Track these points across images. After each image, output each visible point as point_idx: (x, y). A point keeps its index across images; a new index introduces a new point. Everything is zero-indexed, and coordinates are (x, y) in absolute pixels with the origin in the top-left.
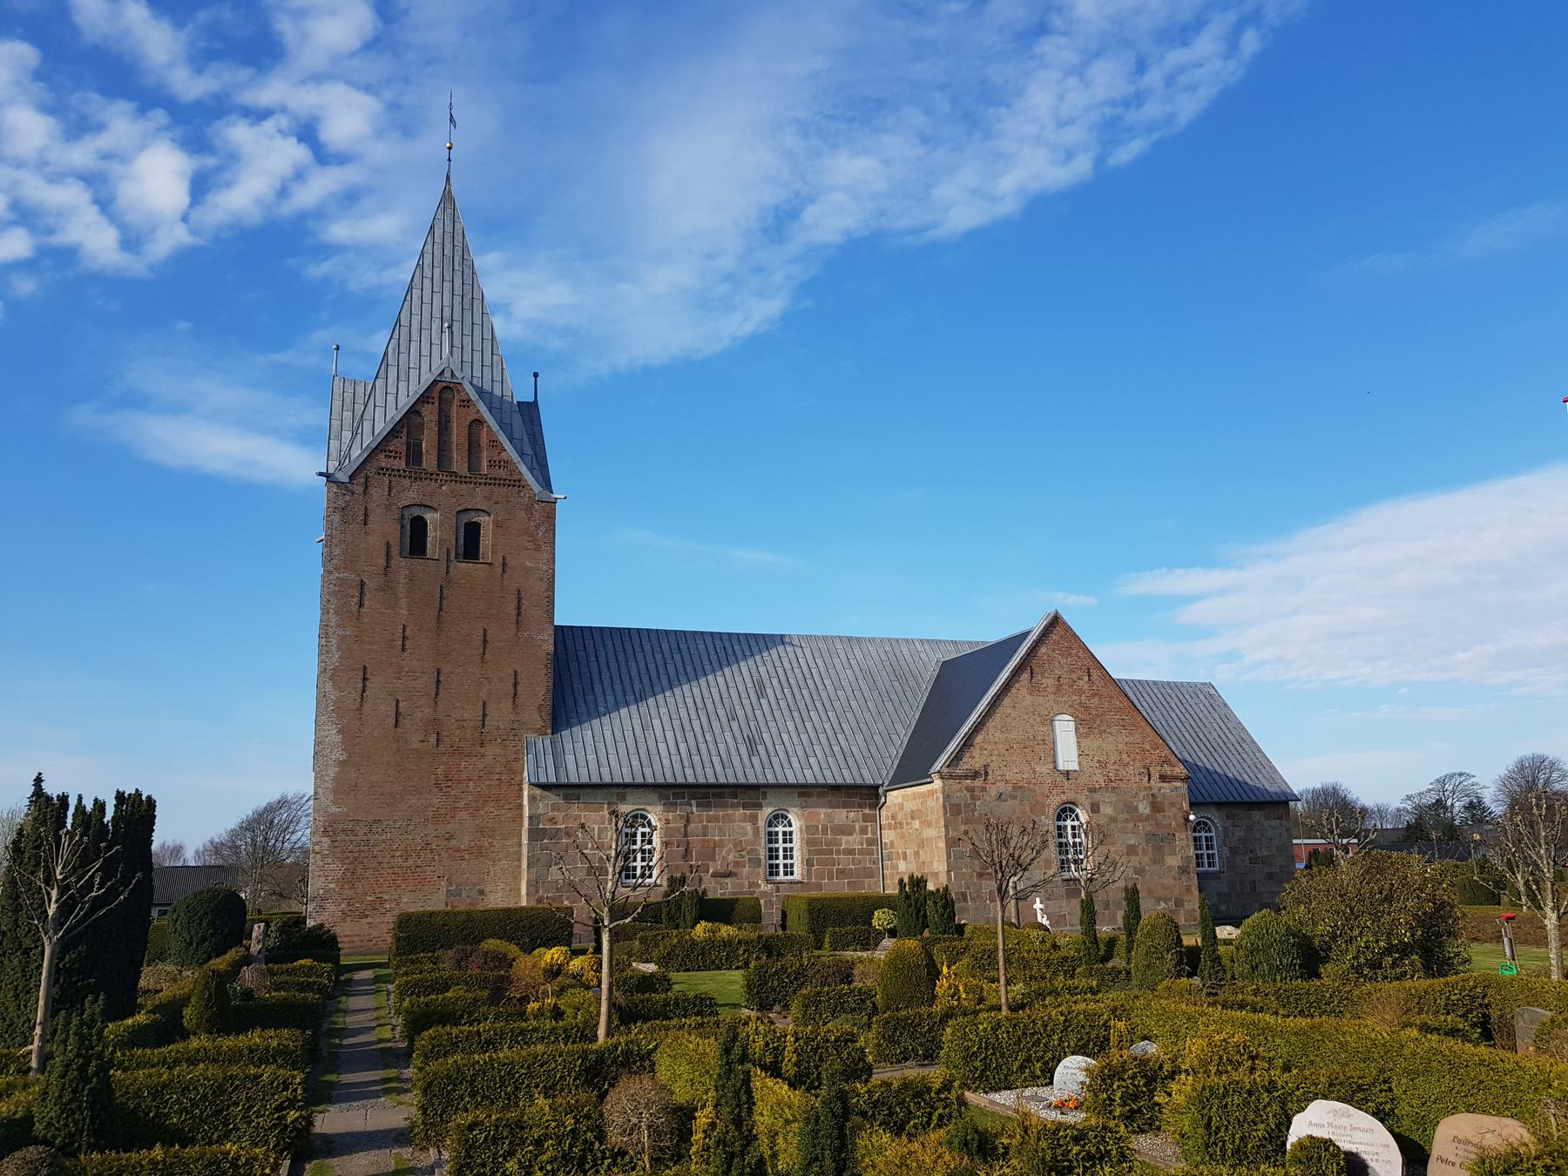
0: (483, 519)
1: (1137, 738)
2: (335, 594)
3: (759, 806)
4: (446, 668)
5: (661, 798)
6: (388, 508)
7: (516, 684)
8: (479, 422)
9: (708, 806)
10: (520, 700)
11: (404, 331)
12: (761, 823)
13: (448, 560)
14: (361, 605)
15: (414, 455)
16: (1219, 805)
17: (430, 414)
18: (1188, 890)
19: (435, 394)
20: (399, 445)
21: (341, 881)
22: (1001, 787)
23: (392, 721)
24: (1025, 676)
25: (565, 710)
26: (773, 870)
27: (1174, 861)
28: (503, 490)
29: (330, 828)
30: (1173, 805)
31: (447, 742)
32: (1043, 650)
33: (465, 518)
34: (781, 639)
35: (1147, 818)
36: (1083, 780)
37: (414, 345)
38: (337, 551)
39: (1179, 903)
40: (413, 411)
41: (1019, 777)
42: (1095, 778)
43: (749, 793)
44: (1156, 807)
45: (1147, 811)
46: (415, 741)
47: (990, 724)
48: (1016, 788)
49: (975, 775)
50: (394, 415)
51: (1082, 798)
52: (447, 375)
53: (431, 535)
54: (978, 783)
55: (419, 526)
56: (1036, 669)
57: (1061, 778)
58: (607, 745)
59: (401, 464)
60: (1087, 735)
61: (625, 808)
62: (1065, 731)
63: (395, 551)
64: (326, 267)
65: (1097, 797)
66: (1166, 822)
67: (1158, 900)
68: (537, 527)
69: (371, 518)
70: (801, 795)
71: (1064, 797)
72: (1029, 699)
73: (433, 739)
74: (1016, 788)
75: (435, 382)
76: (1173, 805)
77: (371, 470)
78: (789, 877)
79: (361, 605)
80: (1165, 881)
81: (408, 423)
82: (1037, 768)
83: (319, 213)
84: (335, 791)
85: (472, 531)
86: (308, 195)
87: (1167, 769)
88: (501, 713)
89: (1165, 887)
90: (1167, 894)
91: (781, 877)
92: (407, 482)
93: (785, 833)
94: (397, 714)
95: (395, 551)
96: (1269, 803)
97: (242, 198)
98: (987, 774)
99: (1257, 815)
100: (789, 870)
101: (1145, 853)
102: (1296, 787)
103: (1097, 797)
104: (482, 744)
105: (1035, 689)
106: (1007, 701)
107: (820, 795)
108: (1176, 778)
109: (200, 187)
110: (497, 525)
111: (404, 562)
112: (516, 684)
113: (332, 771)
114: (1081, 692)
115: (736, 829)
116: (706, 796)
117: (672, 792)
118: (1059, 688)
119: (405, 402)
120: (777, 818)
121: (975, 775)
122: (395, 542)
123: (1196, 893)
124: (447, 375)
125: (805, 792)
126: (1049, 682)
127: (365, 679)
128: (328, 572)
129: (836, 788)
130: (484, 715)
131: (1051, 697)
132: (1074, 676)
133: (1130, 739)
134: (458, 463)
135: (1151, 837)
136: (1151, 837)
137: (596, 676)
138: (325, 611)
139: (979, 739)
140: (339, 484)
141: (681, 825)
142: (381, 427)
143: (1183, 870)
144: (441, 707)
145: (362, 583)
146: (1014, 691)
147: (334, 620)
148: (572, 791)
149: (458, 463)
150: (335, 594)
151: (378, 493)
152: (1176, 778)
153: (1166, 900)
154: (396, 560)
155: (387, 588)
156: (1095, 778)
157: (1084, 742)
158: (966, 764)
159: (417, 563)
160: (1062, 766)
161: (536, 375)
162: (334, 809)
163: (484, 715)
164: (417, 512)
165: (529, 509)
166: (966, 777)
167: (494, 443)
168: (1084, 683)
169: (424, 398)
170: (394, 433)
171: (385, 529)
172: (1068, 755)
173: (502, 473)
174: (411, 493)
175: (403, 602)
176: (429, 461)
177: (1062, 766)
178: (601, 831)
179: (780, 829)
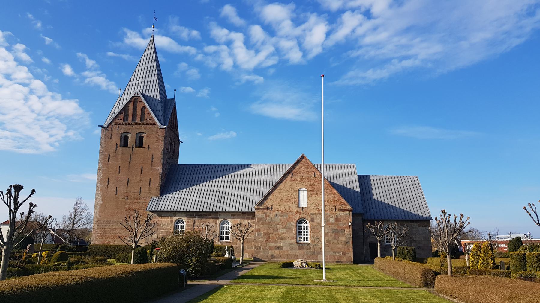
0: (144, 135)
1: (332, 196)
2: (102, 158)
3: (218, 218)
4: (130, 178)
5: (186, 215)
6: (117, 134)
7: (150, 182)
8: (144, 107)
9: (202, 218)
10: (151, 186)
11: (131, 83)
12: (218, 224)
13: (133, 147)
14: (109, 161)
15: (126, 118)
16: (397, 221)
17: (131, 106)
18: (349, 249)
19: (133, 100)
20: (122, 116)
21: (100, 236)
22: (277, 213)
23: (115, 193)
24: (290, 176)
25: (166, 188)
26: (222, 238)
27: (343, 239)
28: (150, 126)
29: (98, 222)
30: (345, 219)
31: (129, 199)
32: (297, 167)
33: (139, 135)
34: (248, 166)
35: (333, 224)
36: (308, 211)
37: (134, 86)
38: (103, 147)
39: (344, 254)
40: (126, 106)
41: (284, 209)
42: (313, 210)
43: (215, 214)
44: (337, 220)
45: (334, 221)
46: (121, 199)
47: (275, 192)
48: (282, 212)
49: (268, 208)
50: (121, 107)
51: (307, 216)
52: (136, 94)
53: (129, 140)
54: (268, 211)
55: (126, 138)
56: (294, 173)
57: (300, 210)
58: (175, 200)
59: (122, 121)
60: (312, 195)
61: (175, 219)
62: (304, 194)
63: (119, 146)
64: (360, 52)
65: (314, 216)
66: (341, 225)
67: (335, 252)
68: (159, 136)
69: (113, 137)
70: (232, 215)
71: (301, 216)
72: (290, 184)
73: (126, 198)
74: (282, 213)
75: (133, 97)
76: (345, 219)
77: (114, 123)
78: (306, 242)
79: (109, 161)
80: (339, 246)
81: (125, 109)
82: (291, 206)
83: (364, 36)
84: (99, 212)
85: (141, 138)
86: (360, 31)
87: (343, 207)
88: (145, 190)
89: (338, 248)
90: (339, 250)
91: (303, 242)
92: (123, 126)
93: (304, 226)
94: (117, 191)
95: (119, 146)
96: (422, 220)
97: (342, 34)
98: (272, 208)
99: (415, 225)
100: (227, 238)
101: (331, 236)
102: (434, 213)
103: (314, 216)
104: (139, 199)
105: (293, 180)
106: (282, 184)
107: (239, 215)
108: (347, 210)
109: (328, 34)
110: (147, 136)
111: (121, 149)
112: (150, 182)
113: (99, 207)
114: (311, 181)
115: (216, 224)
116: (201, 215)
117: (190, 214)
118: (302, 180)
119: (125, 103)
120: (179, 221)
121: (268, 208)
122: (119, 143)
123: (352, 251)
124: (136, 94)
125: (233, 214)
126: (299, 178)
127: (109, 181)
128: (100, 153)
129: (244, 213)
130: (141, 191)
131: (299, 183)
132: (309, 175)
133: (329, 197)
134: (138, 120)
135: (334, 231)
136: (334, 231)
137: (182, 179)
138: (99, 163)
139: (270, 197)
140: (105, 128)
141: (192, 223)
142: (117, 112)
143: (347, 242)
144: (128, 189)
145: (109, 155)
146: (285, 181)
147: (101, 165)
148: (160, 213)
149: (138, 120)
150: (102, 158)
151: (115, 129)
152: (347, 210)
153: (338, 252)
154: (119, 148)
155: (116, 156)
156: (313, 210)
157: (310, 198)
158: (265, 205)
159: (124, 149)
160: (301, 206)
161: (175, 90)
162: (99, 217)
163: (141, 191)
164: (125, 134)
165: (157, 131)
166: (264, 209)
167: (148, 113)
168: (312, 178)
169: (130, 102)
170: (120, 113)
171: (116, 139)
172: (304, 202)
173: (150, 121)
174: (123, 129)
175: (120, 160)
176: (130, 119)
177: (301, 206)
178: (168, 225)
179: (180, 225)
